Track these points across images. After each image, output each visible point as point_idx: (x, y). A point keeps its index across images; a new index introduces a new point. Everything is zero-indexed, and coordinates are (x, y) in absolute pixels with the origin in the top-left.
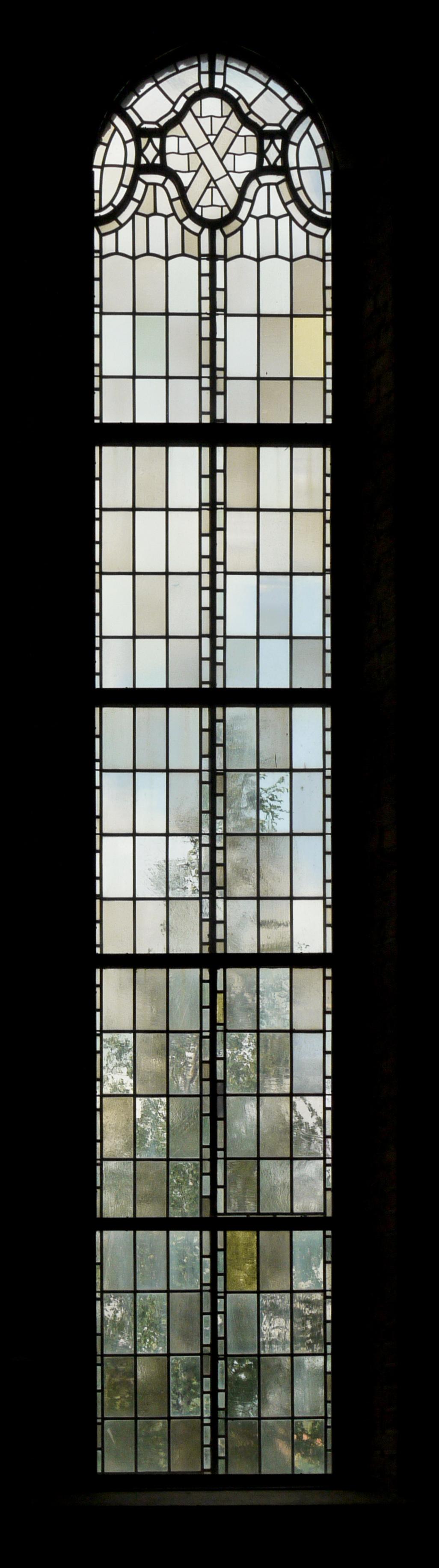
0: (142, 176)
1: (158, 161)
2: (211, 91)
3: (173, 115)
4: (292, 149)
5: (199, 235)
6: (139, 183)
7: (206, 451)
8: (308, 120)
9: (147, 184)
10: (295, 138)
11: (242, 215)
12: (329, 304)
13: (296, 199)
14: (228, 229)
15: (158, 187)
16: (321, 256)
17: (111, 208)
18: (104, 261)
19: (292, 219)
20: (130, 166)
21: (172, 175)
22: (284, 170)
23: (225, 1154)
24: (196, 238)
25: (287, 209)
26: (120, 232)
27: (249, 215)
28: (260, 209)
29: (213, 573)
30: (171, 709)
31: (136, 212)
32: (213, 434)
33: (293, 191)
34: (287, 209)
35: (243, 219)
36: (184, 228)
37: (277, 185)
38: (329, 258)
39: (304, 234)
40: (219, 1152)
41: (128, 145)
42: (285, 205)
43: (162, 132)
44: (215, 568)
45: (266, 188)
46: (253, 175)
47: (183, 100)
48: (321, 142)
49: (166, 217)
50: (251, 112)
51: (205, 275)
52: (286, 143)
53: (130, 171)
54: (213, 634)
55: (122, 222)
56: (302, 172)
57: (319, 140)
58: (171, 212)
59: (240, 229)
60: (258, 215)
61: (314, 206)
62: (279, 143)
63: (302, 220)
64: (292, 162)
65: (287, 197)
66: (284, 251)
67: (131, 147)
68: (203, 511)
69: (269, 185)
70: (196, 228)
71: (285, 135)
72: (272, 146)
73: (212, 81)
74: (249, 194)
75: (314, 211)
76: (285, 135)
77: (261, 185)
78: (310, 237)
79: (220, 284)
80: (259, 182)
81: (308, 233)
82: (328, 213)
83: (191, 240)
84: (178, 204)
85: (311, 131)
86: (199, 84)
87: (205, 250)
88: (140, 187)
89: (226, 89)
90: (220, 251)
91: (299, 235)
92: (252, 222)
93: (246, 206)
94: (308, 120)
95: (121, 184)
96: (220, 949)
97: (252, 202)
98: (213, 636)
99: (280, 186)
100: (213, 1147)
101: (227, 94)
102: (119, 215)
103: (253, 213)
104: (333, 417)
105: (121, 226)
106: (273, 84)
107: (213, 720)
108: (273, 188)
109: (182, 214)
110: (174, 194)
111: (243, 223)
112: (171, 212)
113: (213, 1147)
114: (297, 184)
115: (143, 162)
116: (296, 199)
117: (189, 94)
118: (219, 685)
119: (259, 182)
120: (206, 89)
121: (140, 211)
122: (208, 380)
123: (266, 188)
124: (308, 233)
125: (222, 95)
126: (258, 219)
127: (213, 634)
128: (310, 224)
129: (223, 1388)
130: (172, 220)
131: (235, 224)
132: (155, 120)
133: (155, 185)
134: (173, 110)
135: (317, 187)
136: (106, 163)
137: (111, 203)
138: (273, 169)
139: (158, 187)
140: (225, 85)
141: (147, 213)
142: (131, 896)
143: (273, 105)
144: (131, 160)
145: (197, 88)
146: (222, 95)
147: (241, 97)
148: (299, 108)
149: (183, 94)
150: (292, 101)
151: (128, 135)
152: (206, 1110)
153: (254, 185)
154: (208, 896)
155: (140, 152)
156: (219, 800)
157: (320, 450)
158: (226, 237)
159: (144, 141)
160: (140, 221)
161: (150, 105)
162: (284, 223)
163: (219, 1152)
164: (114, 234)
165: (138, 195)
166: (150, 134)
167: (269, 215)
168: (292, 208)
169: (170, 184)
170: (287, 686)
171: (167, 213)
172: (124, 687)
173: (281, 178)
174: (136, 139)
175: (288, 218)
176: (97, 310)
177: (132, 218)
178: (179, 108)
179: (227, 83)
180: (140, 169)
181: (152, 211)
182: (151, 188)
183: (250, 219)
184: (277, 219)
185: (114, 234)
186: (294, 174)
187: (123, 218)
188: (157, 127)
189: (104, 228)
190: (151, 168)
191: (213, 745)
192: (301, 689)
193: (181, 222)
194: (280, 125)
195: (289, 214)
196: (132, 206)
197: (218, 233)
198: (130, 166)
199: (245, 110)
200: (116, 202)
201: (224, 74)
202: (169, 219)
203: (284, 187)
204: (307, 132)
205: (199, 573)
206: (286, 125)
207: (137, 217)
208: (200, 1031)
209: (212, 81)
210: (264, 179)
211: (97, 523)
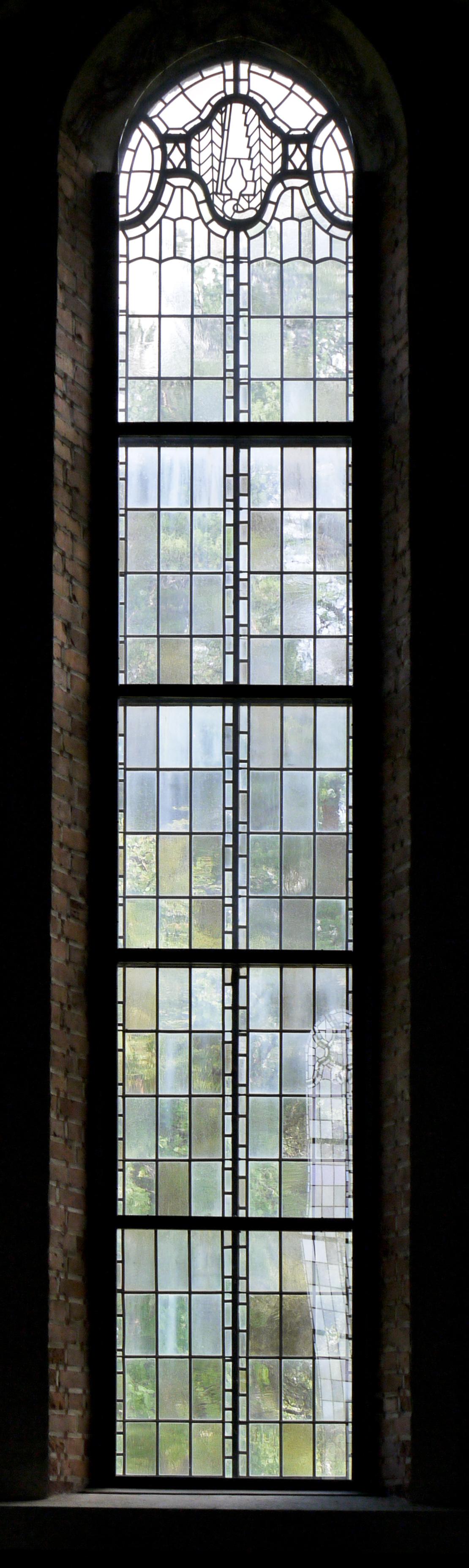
0: (169, 180)
1: (184, 166)
2: (237, 97)
3: (198, 121)
4: (316, 153)
5: (225, 238)
6: (167, 186)
7: (230, 450)
8: (332, 124)
9: (175, 187)
10: (319, 142)
11: (267, 217)
12: (351, 254)
13: (319, 203)
14: (252, 232)
15: (184, 190)
16: (345, 260)
17: (137, 213)
18: (131, 265)
19: (315, 223)
20: (157, 171)
21: (197, 178)
22: (308, 175)
23: (247, 1090)
24: (222, 240)
25: (309, 213)
26: (147, 236)
27: (273, 218)
28: (283, 211)
29: (236, 636)
30: (195, 449)
31: (164, 216)
32: (237, 434)
33: (316, 194)
34: (309, 213)
35: (267, 221)
36: (210, 231)
37: (300, 189)
38: (351, 260)
39: (328, 237)
40: (230, 1039)
41: (155, 151)
42: (308, 209)
43: (187, 138)
44: (238, 765)
45: (290, 191)
46: (278, 178)
47: (209, 109)
48: (345, 146)
49: (193, 221)
50: (276, 117)
51: (230, 276)
52: (310, 148)
53: (156, 176)
54: (235, 378)
55: (149, 226)
56: (326, 175)
57: (342, 144)
58: (198, 215)
59: (264, 232)
60: (281, 218)
61: (337, 209)
62: (304, 147)
63: (326, 224)
64: (316, 167)
65: (310, 201)
66: (307, 253)
67: (158, 153)
68: (245, 1029)
69: (292, 188)
70: (222, 231)
71: (309, 139)
72: (298, 150)
73: (236, 88)
74: (273, 197)
75: (337, 214)
76: (309, 139)
77: (286, 189)
78: (333, 239)
79: (242, 1448)
80: (284, 185)
81: (332, 236)
82: (349, 216)
83: (217, 243)
84: (204, 207)
85: (333, 134)
86: (224, 91)
87: (230, 252)
88: (168, 189)
89: (251, 95)
90: (243, 253)
91: (322, 238)
92: (275, 224)
93: (270, 208)
94: (332, 124)
95: (148, 190)
96: (242, 1214)
97: (276, 204)
98: (236, 1423)
99: (303, 190)
100: (235, 1277)
101: (252, 100)
102: (147, 219)
103: (276, 216)
104: (355, 941)
105: (148, 230)
106: (298, 89)
107: (236, 977)
108: (296, 192)
109: (207, 216)
110: (201, 197)
111: (268, 225)
112: (198, 215)
113: (235, 1277)
114: (320, 188)
115: (169, 166)
116: (319, 203)
117: (213, 102)
118: (243, 681)
119: (284, 185)
120: (231, 95)
121: (167, 215)
122: (230, 1162)
123: (290, 191)
124: (332, 236)
125: (247, 101)
126: (281, 221)
127: (236, 633)
128: (334, 228)
129: (245, 1328)
130: (199, 224)
131: (260, 227)
132: (181, 126)
133: (182, 188)
134: (199, 117)
135: (339, 190)
136: (134, 169)
137: (138, 209)
138: (297, 173)
139: (184, 190)
140: (249, 90)
141: (174, 217)
142: (157, 313)
143: (298, 108)
144: (158, 167)
145: (223, 95)
146: (247, 101)
147: (266, 101)
148: (324, 112)
149: (209, 103)
150: (316, 104)
151: (155, 142)
152: (229, 1109)
153: (279, 188)
154: (232, 260)
155: (165, 157)
156: (243, 604)
157: (344, 449)
158: (249, 239)
159: (169, 146)
160: (167, 225)
161: (176, 110)
162: (307, 225)
163: (230, 1039)
164: (141, 238)
165: (165, 199)
166: (176, 140)
167: (292, 218)
168: (315, 211)
169: (196, 187)
170: (312, 420)
171: (193, 217)
172: (325, 421)
173: (306, 182)
174: (163, 147)
175: (310, 222)
176: (119, 1353)
177: (159, 222)
178: (204, 116)
179: (251, 88)
180: (165, 174)
181: (178, 222)
182: (178, 191)
183: (274, 221)
184: (300, 221)
185: (141, 238)
186: (318, 177)
187: (150, 222)
188: (183, 133)
189: (131, 233)
190: (177, 172)
191: (235, 1193)
192: (327, 423)
193: (206, 224)
194: (306, 129)
195: (311, 217)
196: (160, 210)
197: (242, 235)
198: (157, 171)
199: (270, 115)
200: (142, 208)
201: (248, 80)
202: (195, 222)
203: (307, 191)
204: (330, 135)
205: (224, 769)
206: (311, 129)
207: (164, 220)
208: (224, 316)
209: (236, 88)
210: (289, 183)
211: (350, 989)
